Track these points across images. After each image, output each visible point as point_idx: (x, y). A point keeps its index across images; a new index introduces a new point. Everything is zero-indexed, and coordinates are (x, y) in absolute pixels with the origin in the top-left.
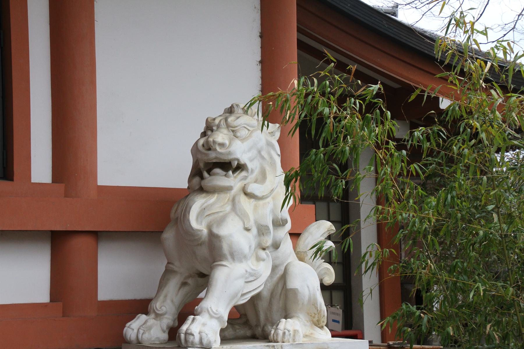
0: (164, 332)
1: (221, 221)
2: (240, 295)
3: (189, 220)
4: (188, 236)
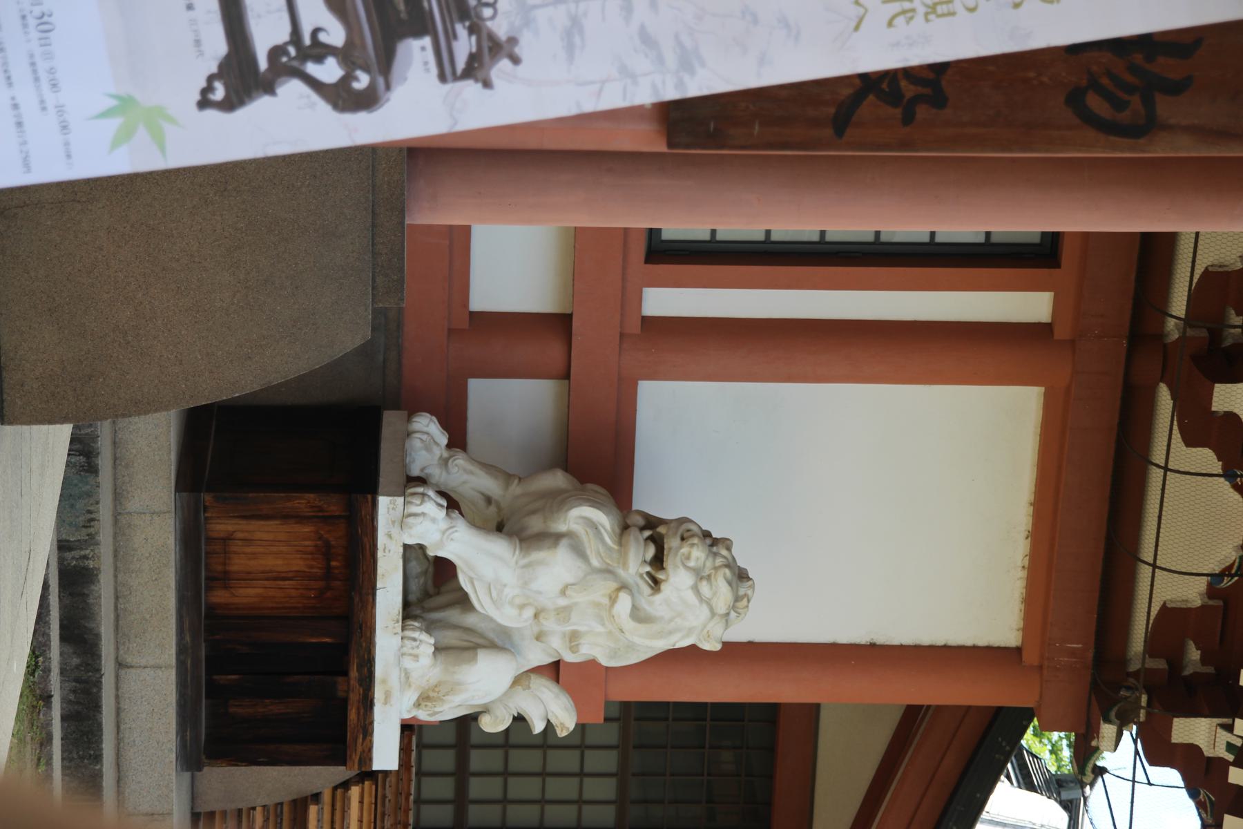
0: (422, 470)
1: (579, 551)
2: (473, 575)
3: (581, 505)
4: (557, 501)
